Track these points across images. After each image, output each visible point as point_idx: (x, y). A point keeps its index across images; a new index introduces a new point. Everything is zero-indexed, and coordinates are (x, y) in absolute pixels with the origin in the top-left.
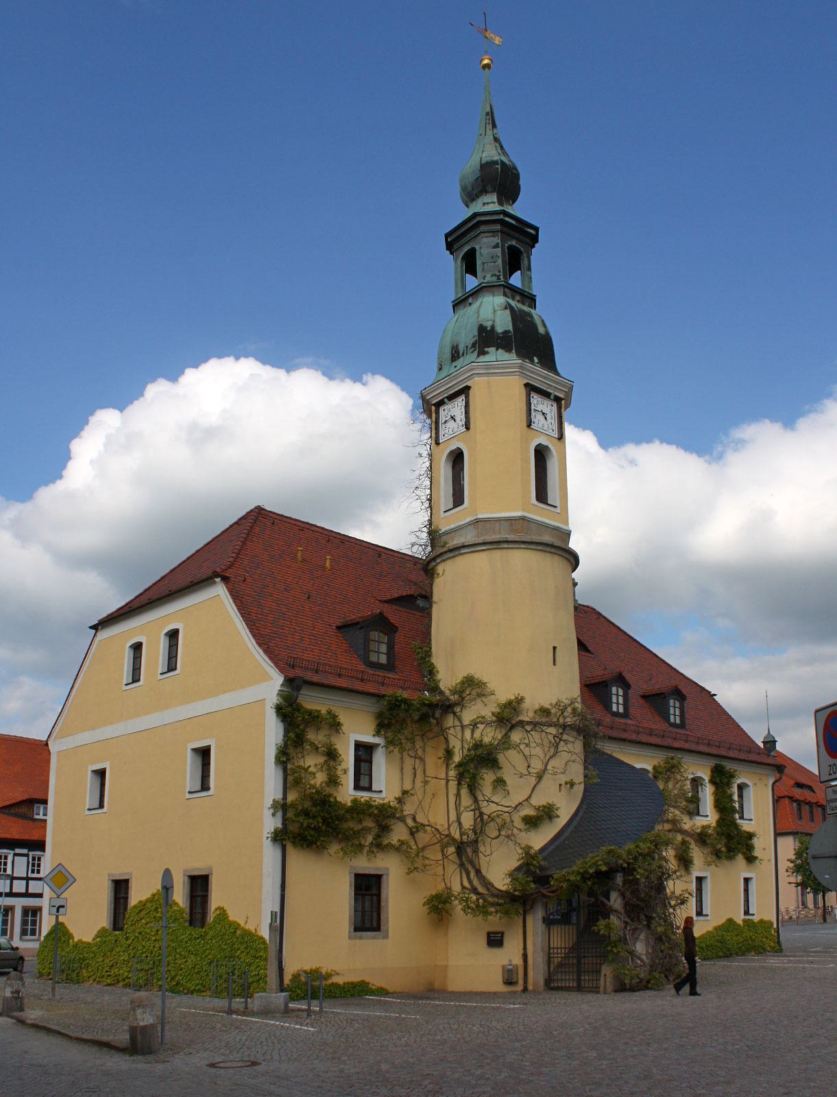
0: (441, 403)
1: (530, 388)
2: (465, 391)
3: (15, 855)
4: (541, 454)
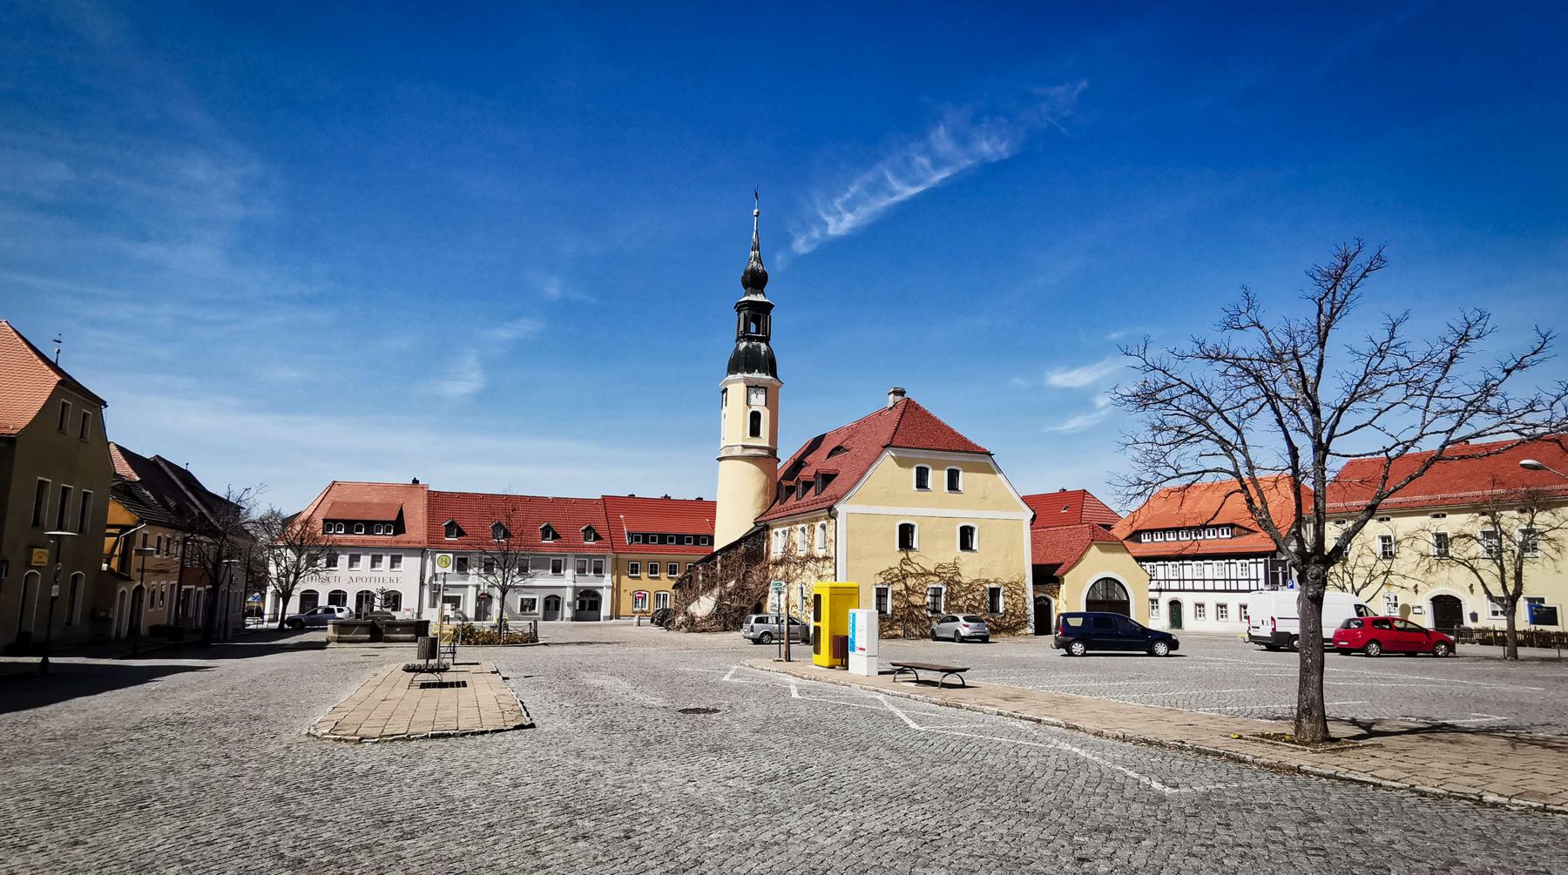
1: (748, 387)
3: (1250, 563)
4: (755, 417)
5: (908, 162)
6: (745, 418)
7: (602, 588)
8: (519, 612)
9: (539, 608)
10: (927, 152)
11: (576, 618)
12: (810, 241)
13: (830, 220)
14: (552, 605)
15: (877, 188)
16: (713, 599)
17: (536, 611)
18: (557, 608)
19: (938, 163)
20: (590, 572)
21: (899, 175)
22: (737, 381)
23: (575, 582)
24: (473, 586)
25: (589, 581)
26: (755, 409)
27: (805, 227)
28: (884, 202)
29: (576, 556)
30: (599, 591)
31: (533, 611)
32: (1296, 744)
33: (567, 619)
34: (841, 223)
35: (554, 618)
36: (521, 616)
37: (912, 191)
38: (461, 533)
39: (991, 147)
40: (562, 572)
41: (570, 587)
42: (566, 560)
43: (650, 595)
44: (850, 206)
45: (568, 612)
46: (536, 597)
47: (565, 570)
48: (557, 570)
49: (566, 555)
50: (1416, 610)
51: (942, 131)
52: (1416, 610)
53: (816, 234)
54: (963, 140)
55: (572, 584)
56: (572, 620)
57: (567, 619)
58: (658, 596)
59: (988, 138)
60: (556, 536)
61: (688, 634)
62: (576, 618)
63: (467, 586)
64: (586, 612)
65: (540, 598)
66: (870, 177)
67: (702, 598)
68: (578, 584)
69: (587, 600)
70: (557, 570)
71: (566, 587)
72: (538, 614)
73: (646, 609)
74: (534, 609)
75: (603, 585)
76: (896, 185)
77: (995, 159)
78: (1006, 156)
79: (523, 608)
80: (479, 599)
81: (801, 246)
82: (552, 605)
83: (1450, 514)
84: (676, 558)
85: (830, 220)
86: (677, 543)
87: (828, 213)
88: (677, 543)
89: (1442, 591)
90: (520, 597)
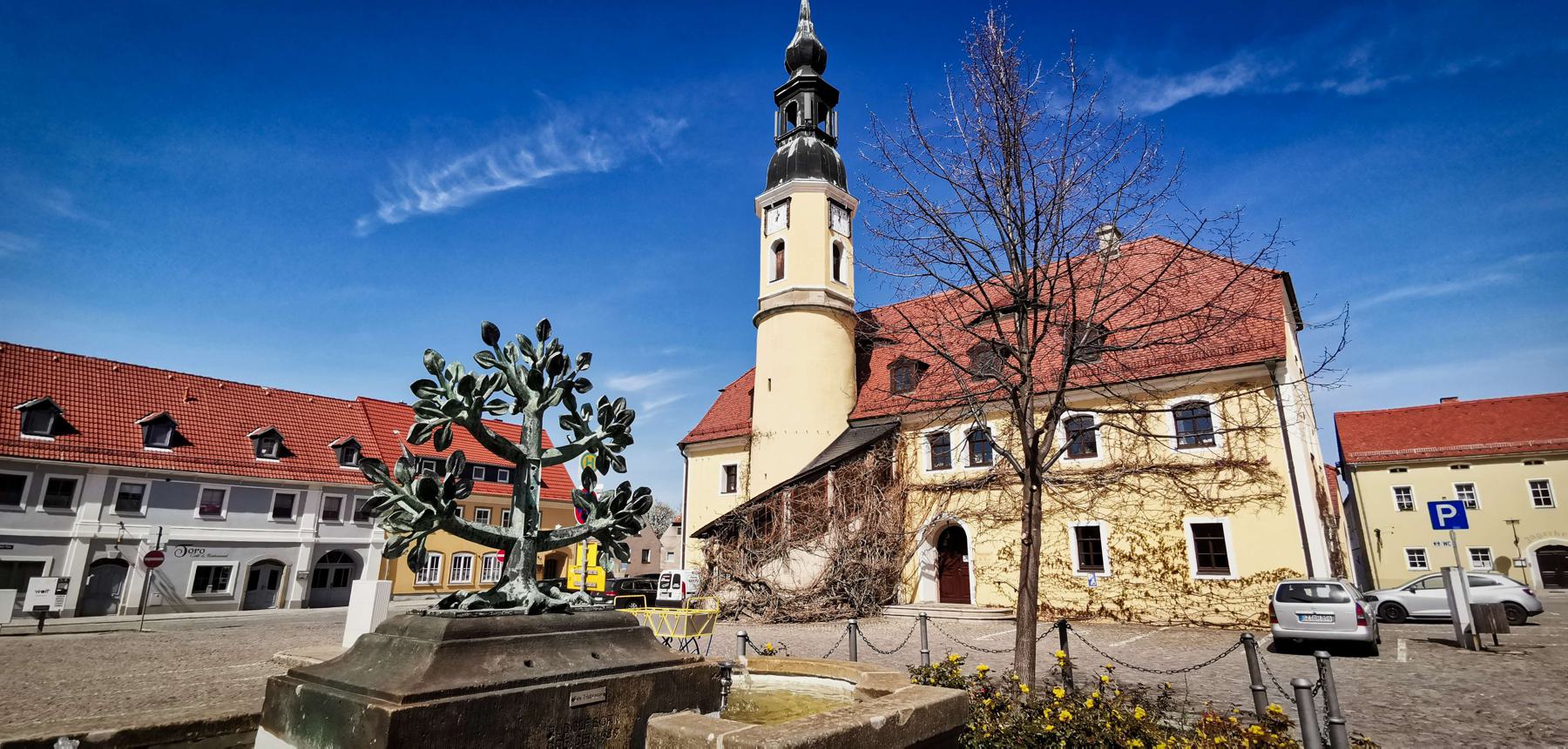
0: (768, 208)
2: (788, 200)
5: (513, 153)
6: (827, 248)
7: (366, 546)
8: (188, 593)
9: (235, 586)
10: (534, 148)
11: (310, 602)
12: (398, 212)
13: (424, 195)
14: (264, 579)
15: (478, 172)
16: (824, 554)
17: (229, 590)
18: (273, 584)
19: (542, 162)
20: (347, 518)
21: (502, 164)
22: (814, 189)
23: (317, 535)
24: (83, 540)
25: (344, 534)
26: (837, 238)
27: (394, 196)
28: (483, 189)
29: (325, 489)
30: (360, 551)
31: (220, 592)
32: (200, 640)
33: (294, 605)
34: (434, 202)
35: (266, 604)
36: (194, 602)
37: (514, 183)
38: (63, 428)
39: (595, 158)
40: (294, 517)
41: (307, 544)
42: (304, 496)
43: (445, 559)
44: (446, 185)
45: (297, 591)
46: (235, 564)
47: (300, 514)
48: (283, 511)
49: (306, 487)
50: (1518, 563)
51: (549, 130)
52: (1518, 563)
53: (407, 206)
54: (570, 147)
55: (311, 538)
56: (306, 604)
57: (294, 605)
58: (457, 561)
59: (593, 151)
60: (284, 452)
61: (774, 627)
62: (310, 602)
63: (65, 541)
64: (328, 591)
65: (238, 567)
66: (471, 159)
67: (794, 553)
68: (323, 540)
69: (332, 568)
70: (283, 511)
71: (298, 544)
72: (231, 598)
73: (437, 582)
74: (224, 587)
75: (370, 540)
76: (497, 174)
77: (595, 171)
78: (605, 169)
79: (199, 586)
80: (93, 566)
81: (387, 213)
82: (264, 579)
83: (1548, 460)
84: (490, 500)
85: (424, 195)
86: (486, 480)
87: (422, 188)
88: (486, 480)
89: (1550, 541)
90: (195, 564)
